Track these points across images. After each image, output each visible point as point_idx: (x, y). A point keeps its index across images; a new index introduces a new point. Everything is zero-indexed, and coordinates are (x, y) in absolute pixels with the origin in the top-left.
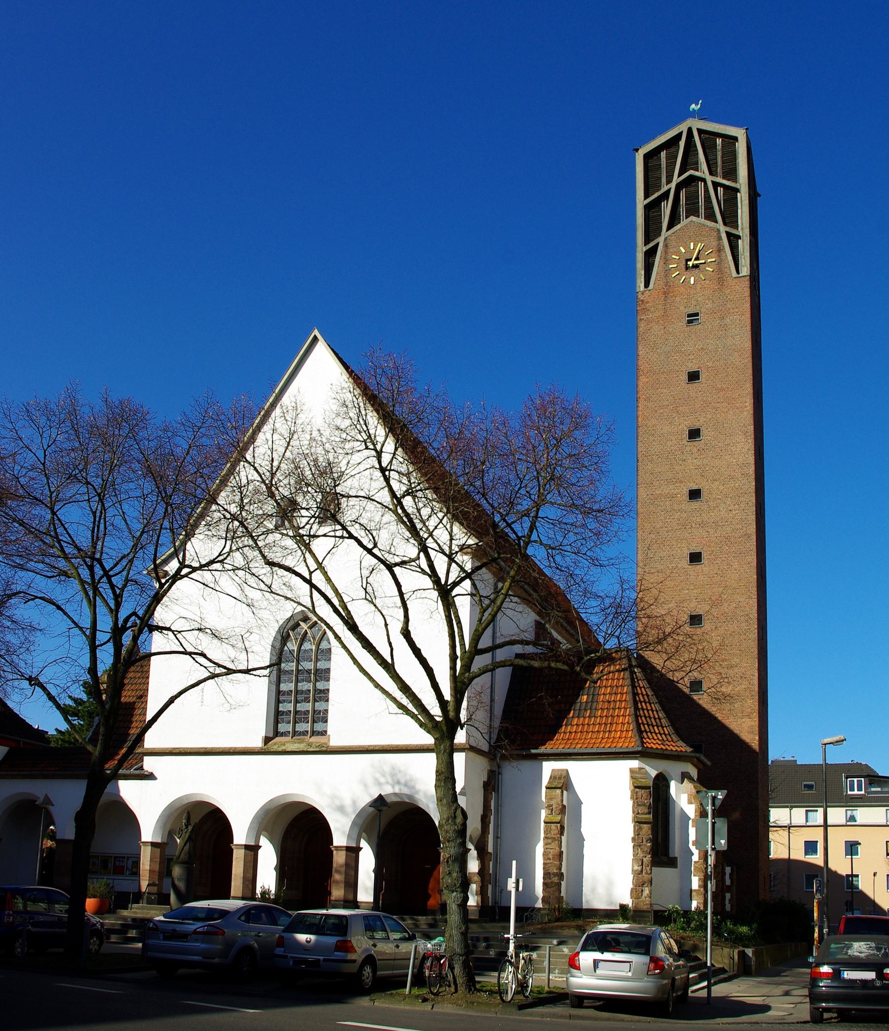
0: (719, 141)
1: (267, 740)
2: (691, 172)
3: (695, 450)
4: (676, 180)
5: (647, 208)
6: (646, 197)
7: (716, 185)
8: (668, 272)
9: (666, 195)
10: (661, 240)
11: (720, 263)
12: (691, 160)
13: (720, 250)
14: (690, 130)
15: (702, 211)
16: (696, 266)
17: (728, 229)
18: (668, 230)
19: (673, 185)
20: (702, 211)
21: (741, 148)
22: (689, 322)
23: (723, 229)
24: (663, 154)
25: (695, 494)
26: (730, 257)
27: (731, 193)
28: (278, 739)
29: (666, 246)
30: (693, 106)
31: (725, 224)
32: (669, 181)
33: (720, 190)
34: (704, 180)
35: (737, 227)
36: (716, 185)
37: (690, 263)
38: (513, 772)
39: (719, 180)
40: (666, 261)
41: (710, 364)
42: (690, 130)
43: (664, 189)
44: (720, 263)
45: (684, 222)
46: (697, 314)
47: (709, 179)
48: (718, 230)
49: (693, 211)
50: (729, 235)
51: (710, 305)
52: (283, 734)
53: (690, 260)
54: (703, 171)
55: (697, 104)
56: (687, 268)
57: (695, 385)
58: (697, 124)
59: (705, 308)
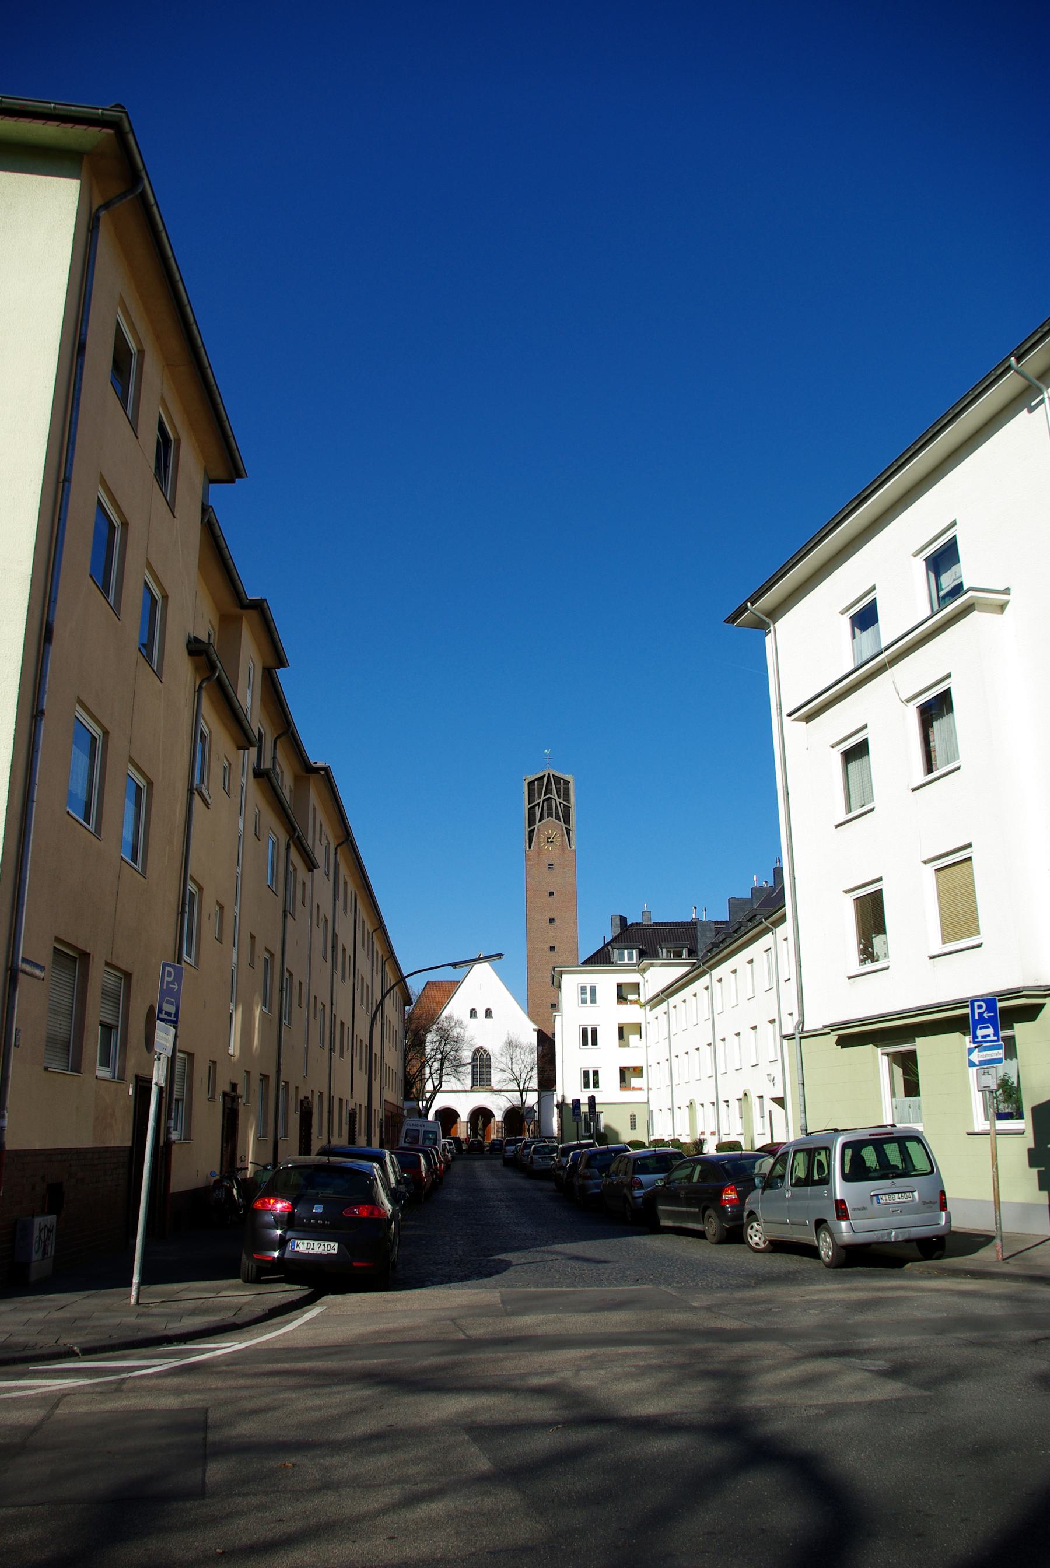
0: (562, 781)
1: (472, 1087)
2: (549, 795)
3: (552, 929)
4: (543, 798)
5: (530, 809)
6: (529, 804)
7: (560, 803)
8: (540, 843)
9: (539, 804)
10: (536, 826)
11: (563, 841)
12: (550, 787)
13: (563, 835)
14: (549, 774)
15: (554, 814)
16: (552, 842)
17: (567, 826)
18: (539, 821)
19: (541, 800)
20: (554, 814)
21: (572, 786)
22: (549, 868)
23: (564, 825)
24: (536, 782)
25: (552, 949)
26: (567, 840)
27: (567, 808)
28: (474, 1087)
29: (538, 829)
30: (546, 751)
31: (565, 823)
32: (539, 798)
33: (562, 805)
34: (556, 800)
35: (570, 826)
36: (560, 803)
37: (550, 840)
38: (543, 1094)
39: (562, 801)
40: (539, 837)
41: (558, 889)
42: (549, 774)
43: (538, 801)
44: (563, 841)
45: (546, 820)
46: (552, 865)
47: (558, 800)
48: (562, 826)
49: (550, 815)
50: (566, 828)
51: (559, 861)
52: (476, 1085)
53: (550, 838)
54: (555, 795)
55: (548, 751)
56: (548, 842)
57: (552, 953)
58: (553, 772)
59: (556, 862)
